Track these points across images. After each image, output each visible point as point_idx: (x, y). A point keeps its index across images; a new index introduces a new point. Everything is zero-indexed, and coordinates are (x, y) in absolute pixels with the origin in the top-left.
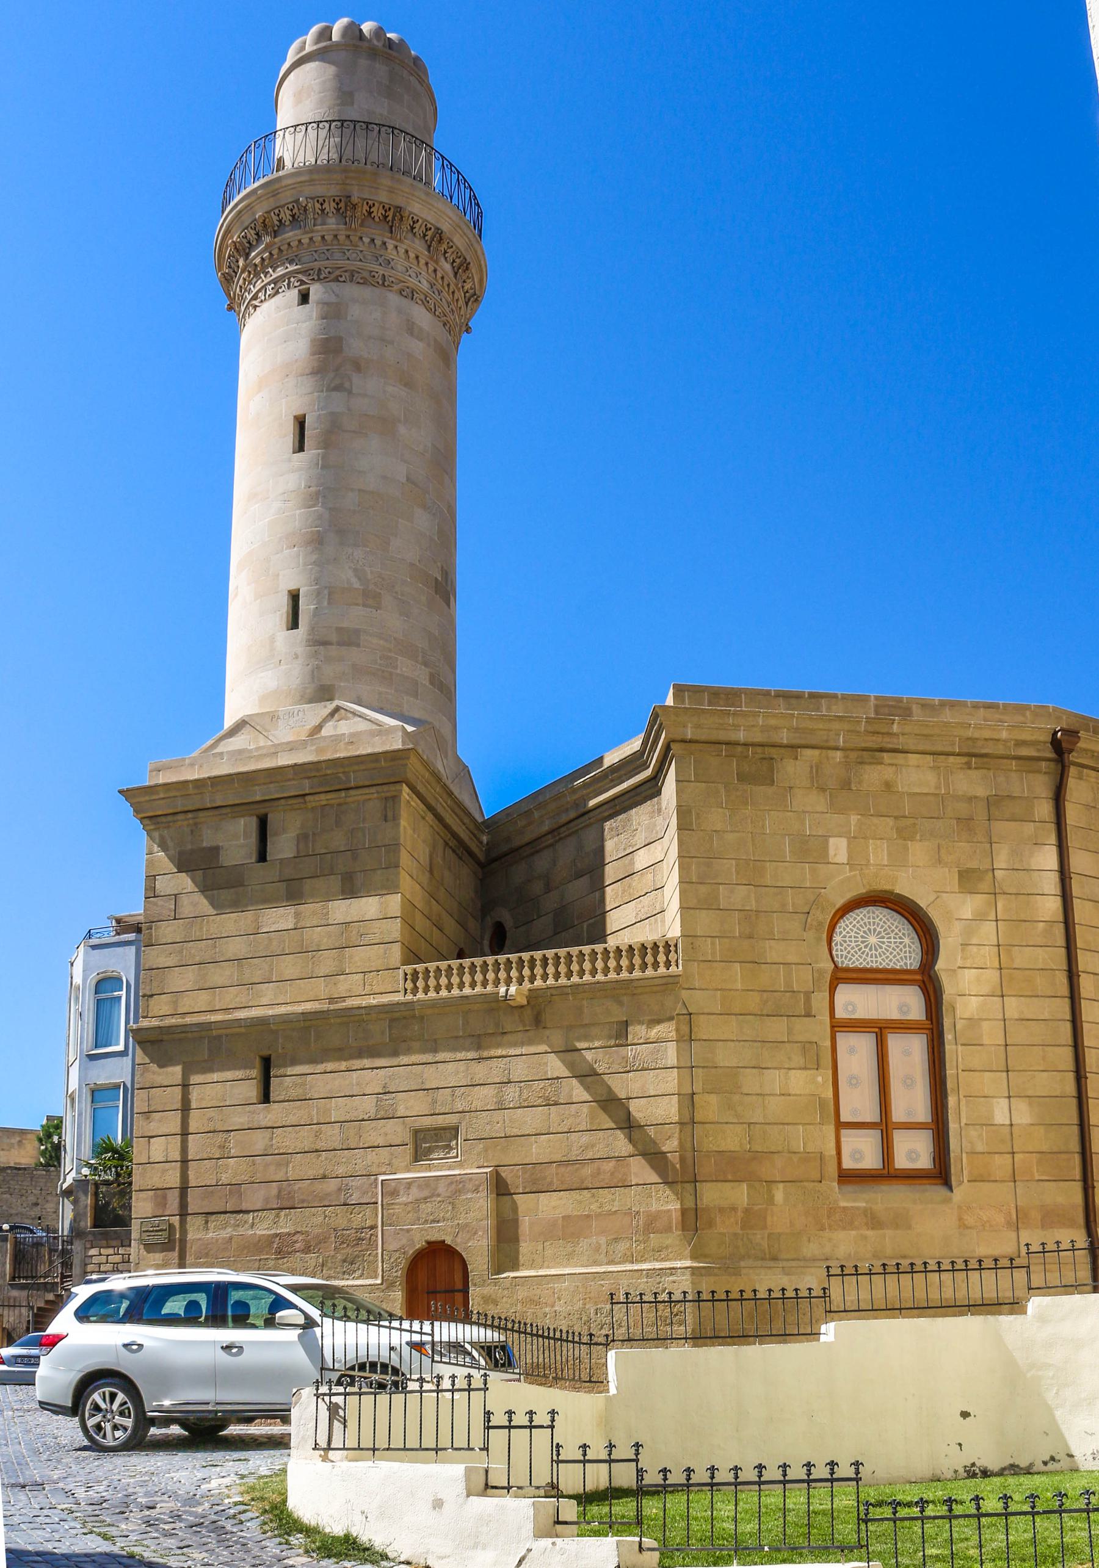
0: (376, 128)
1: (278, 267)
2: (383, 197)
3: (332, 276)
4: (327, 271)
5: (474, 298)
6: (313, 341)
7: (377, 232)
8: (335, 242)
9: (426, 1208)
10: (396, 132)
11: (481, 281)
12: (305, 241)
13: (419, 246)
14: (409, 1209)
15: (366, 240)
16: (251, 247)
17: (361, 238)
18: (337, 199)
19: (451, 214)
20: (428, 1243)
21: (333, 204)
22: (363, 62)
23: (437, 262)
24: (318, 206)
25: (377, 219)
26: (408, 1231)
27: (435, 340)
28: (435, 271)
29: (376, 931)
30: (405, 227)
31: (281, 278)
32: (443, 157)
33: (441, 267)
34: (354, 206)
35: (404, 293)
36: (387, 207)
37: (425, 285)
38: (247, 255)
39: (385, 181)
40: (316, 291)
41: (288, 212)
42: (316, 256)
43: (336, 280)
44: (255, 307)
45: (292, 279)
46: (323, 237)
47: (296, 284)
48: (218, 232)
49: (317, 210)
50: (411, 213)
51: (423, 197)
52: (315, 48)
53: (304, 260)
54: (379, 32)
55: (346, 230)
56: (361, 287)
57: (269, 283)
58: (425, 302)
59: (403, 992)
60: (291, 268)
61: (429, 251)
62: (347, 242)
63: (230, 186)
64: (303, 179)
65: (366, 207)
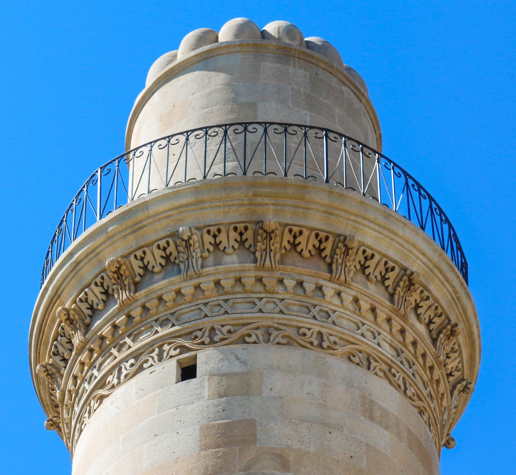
0: (301, 132)
1: (140, 333)
2: (316, 221)
3: (234, 337)
4: (225, 330)
5: (462, 386)
6: (204, 430)
7: (307, 271)
8: (238, 289)
10: (331, 135)
11: (472, 358)
12: (188, 289)
13: (375, 292)
15: (290, 283)
16: (94, 312)
17: (281, 281)
18: (241, 227)
19: (423, 246)
21: (234, 235)
22: (270, 66)
23: (404, 318)
24: (208, 239)
25: (306, 254)
27: (409, 431)
28: (402, 332)
30: (353, 262)
31: (149, 347)
32: (406, 174)
33: (412, 327)
34: (269, 235)
35: (356, 360)
37: (388, 351)
38: (88, 327)
39: (320, 197)
40: (207, 359)
41: (158, 253)
42: (206, 310)
43: (242, 340)
44: (102, 398)
45: (166, 347)
46: (217, 283)
47: (173, 353)
48: (39, 303)
49: (208, 246)
50: (361, 244)
51: (381, 220)
52: (193, 53)
53: (185, 317)
54: (290, 31)
55: (257, 269)
56: (285, 348)
57: (125, 359)
58: (388, 375)
60: (163, 332)
61: (392, 301)
62: (259, 287)
63: (57, 242)
64: (184, 201)
65: (288, 237)
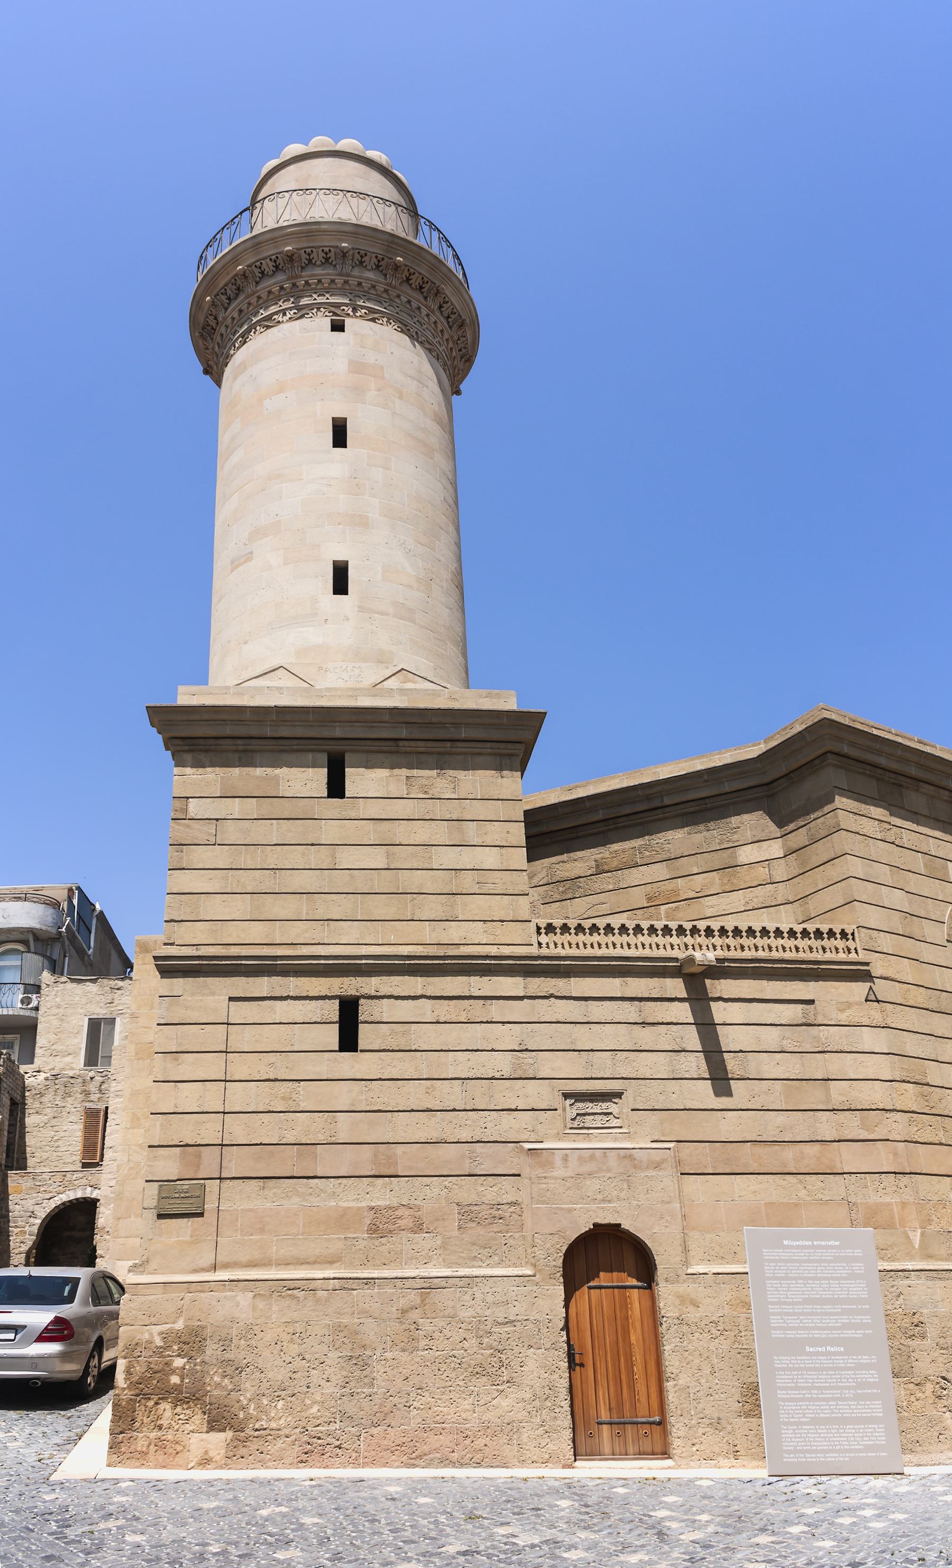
9: (592, 1186)
14: (568, 1184)
15: (404, 299)
20: (595, 1225)
25: (319, 263)
26: (570, 1210)
29: (497, 881)
36: (426, 279)
44: (268, 327)
59: (536, 945)
